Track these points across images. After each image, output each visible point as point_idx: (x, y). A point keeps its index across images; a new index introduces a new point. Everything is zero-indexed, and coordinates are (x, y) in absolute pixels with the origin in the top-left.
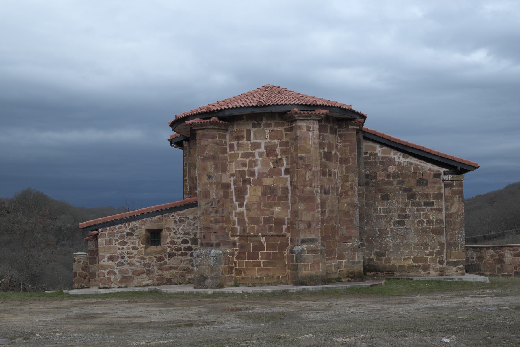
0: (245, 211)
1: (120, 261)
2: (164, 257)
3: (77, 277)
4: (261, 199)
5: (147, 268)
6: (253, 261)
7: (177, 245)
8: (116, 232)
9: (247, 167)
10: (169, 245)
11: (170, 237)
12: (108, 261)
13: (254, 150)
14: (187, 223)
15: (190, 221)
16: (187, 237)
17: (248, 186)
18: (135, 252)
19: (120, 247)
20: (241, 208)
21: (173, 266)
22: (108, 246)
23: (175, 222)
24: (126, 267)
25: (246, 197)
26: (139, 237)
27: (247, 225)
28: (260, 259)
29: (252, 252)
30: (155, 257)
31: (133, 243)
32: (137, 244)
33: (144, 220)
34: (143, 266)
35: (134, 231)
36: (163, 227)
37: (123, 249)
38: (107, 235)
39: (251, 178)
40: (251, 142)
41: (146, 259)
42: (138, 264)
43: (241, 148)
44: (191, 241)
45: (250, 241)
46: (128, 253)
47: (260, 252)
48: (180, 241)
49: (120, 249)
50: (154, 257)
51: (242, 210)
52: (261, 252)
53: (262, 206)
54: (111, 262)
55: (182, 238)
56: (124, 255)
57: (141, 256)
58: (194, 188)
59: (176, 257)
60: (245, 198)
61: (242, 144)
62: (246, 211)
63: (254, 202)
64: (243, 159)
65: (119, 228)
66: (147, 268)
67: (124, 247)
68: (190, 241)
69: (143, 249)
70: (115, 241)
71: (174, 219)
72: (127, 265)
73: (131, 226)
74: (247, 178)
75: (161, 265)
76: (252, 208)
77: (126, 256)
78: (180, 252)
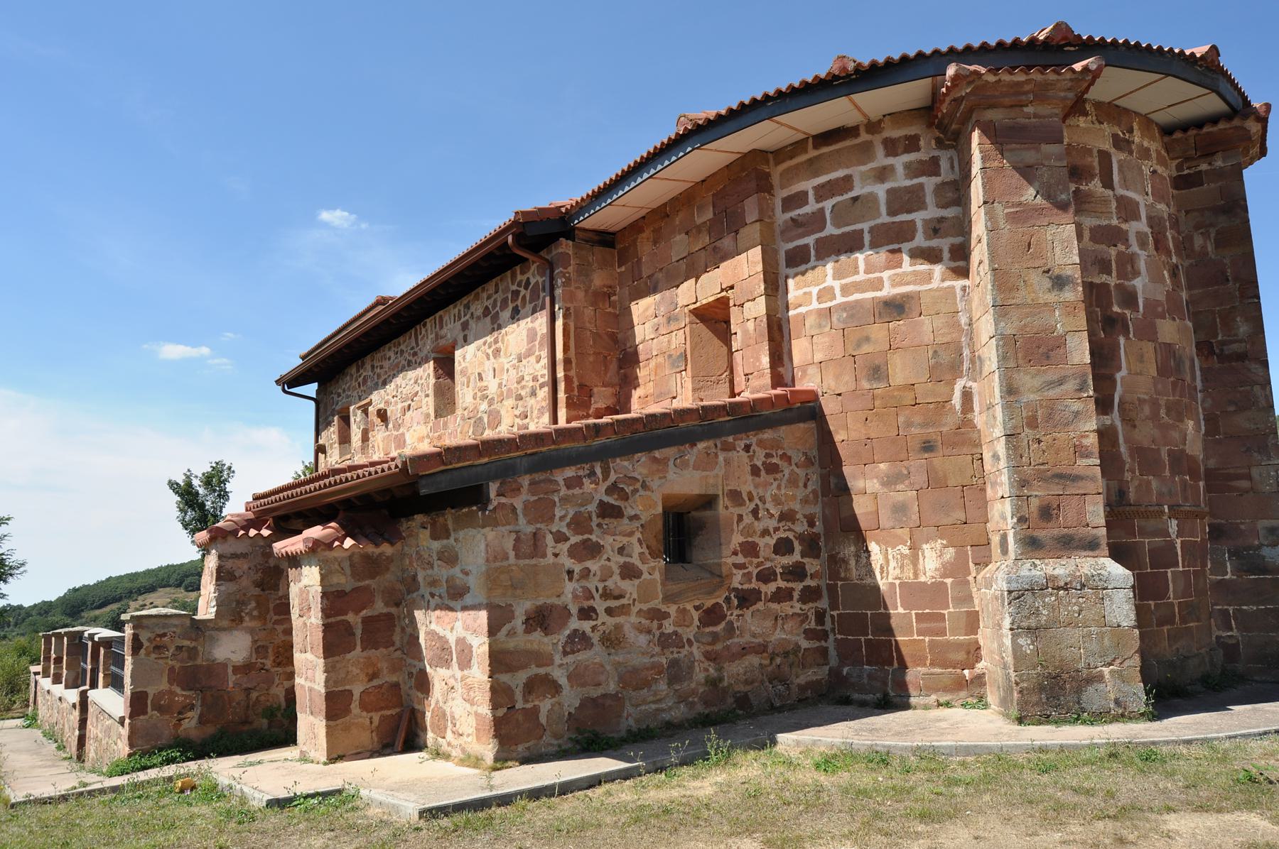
0: (1118, 423)
1: (576, 631)
2: (725, 609)
3: (145, 713)
4: (1160, 386)
5: (672, 652)
6: (1155, 605)
7: (761, 559)
8: (557, 499)
9: (1114, 274)
10: (740, 559)
11: (741, 527)
12: (528, 631)
13: (1126, 221)
14: (787, 476)
15: (796, 469)
16: (790, 530)
17: (1122, 340)
18: (629, 587)
19: (577, 568)
20: (1107, 414)
21: (754, 640)
22: (527, 561)
23: (755, 471)
24: (594, 655)
25: (1118, 376)
26: (642, 525)
27: (1128, 476)
28: (1172, 596)
29: (1149, 570)
30: (697, 608)
31: (621, 551)
32: (636, 555)
33: (657, 454)
34: (657, 649)
35: (625, 497)
36: (720, 488)
37: (586, 573)
38: (519, 511)
39: (1128, 312)
40: (1115, 195)
41: (666, 615)
42: (643, 639)
43: (1086, 206)
44: (800, 544)
45: (1143, 533)
46: (606, 595)
47: (1169, 571)
48: (772, 541)
49: (576, 576)
50: (694, 606)
51: (1108, 422)
52: (1173, 569)
53: (1163, 412)
54: (537, 635)
55: (775, 533)
56: (592, 601)
57: (652, 605)
58: (776, 358)
59: (760, 606)
60: (1114, 381)
61: (1089, 194)
62: (1122, 425)
63: (1142, 396)
64: (1097, 246)
65: (570, 484)
66: (672, 652)
67: (594, 566)
68: (796, 544)
69: (657, 576)
70: (557, 541)
71: (751, 458)
72: (598, 648)
73: (613, 477)
74: (1116, 312)
75: (715, 638)
76: (1137, 414)
77: (600, 605)
78: (770, 588)
